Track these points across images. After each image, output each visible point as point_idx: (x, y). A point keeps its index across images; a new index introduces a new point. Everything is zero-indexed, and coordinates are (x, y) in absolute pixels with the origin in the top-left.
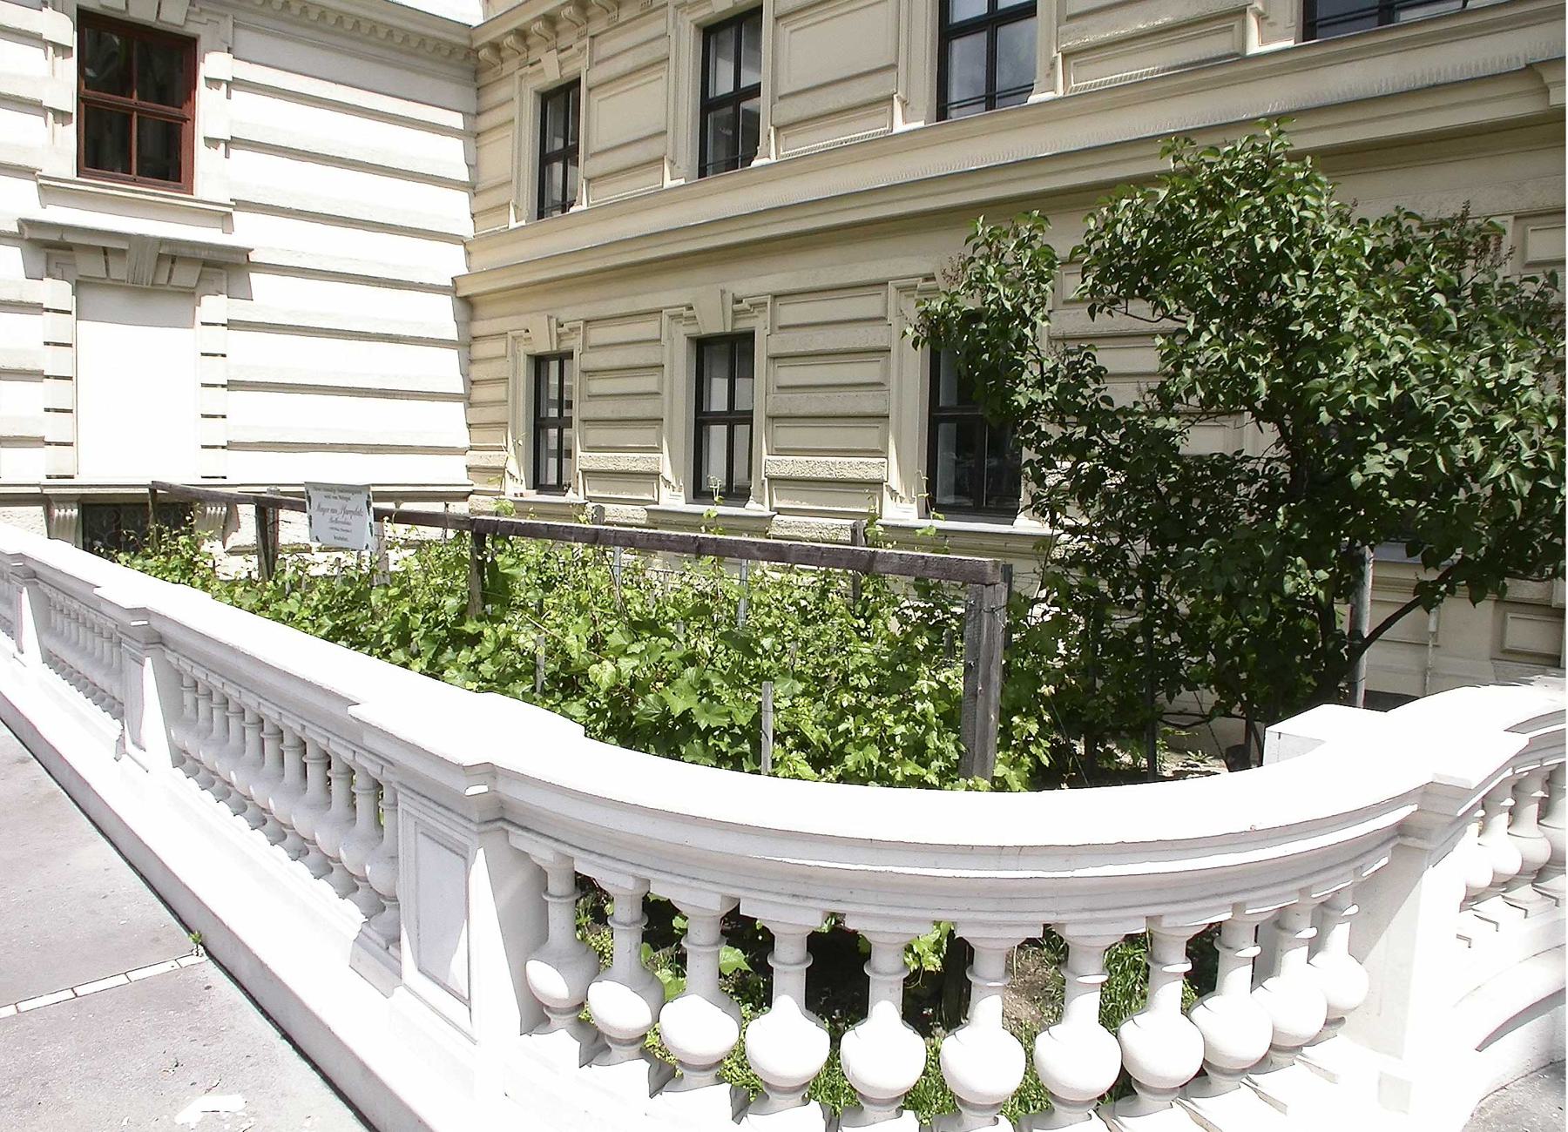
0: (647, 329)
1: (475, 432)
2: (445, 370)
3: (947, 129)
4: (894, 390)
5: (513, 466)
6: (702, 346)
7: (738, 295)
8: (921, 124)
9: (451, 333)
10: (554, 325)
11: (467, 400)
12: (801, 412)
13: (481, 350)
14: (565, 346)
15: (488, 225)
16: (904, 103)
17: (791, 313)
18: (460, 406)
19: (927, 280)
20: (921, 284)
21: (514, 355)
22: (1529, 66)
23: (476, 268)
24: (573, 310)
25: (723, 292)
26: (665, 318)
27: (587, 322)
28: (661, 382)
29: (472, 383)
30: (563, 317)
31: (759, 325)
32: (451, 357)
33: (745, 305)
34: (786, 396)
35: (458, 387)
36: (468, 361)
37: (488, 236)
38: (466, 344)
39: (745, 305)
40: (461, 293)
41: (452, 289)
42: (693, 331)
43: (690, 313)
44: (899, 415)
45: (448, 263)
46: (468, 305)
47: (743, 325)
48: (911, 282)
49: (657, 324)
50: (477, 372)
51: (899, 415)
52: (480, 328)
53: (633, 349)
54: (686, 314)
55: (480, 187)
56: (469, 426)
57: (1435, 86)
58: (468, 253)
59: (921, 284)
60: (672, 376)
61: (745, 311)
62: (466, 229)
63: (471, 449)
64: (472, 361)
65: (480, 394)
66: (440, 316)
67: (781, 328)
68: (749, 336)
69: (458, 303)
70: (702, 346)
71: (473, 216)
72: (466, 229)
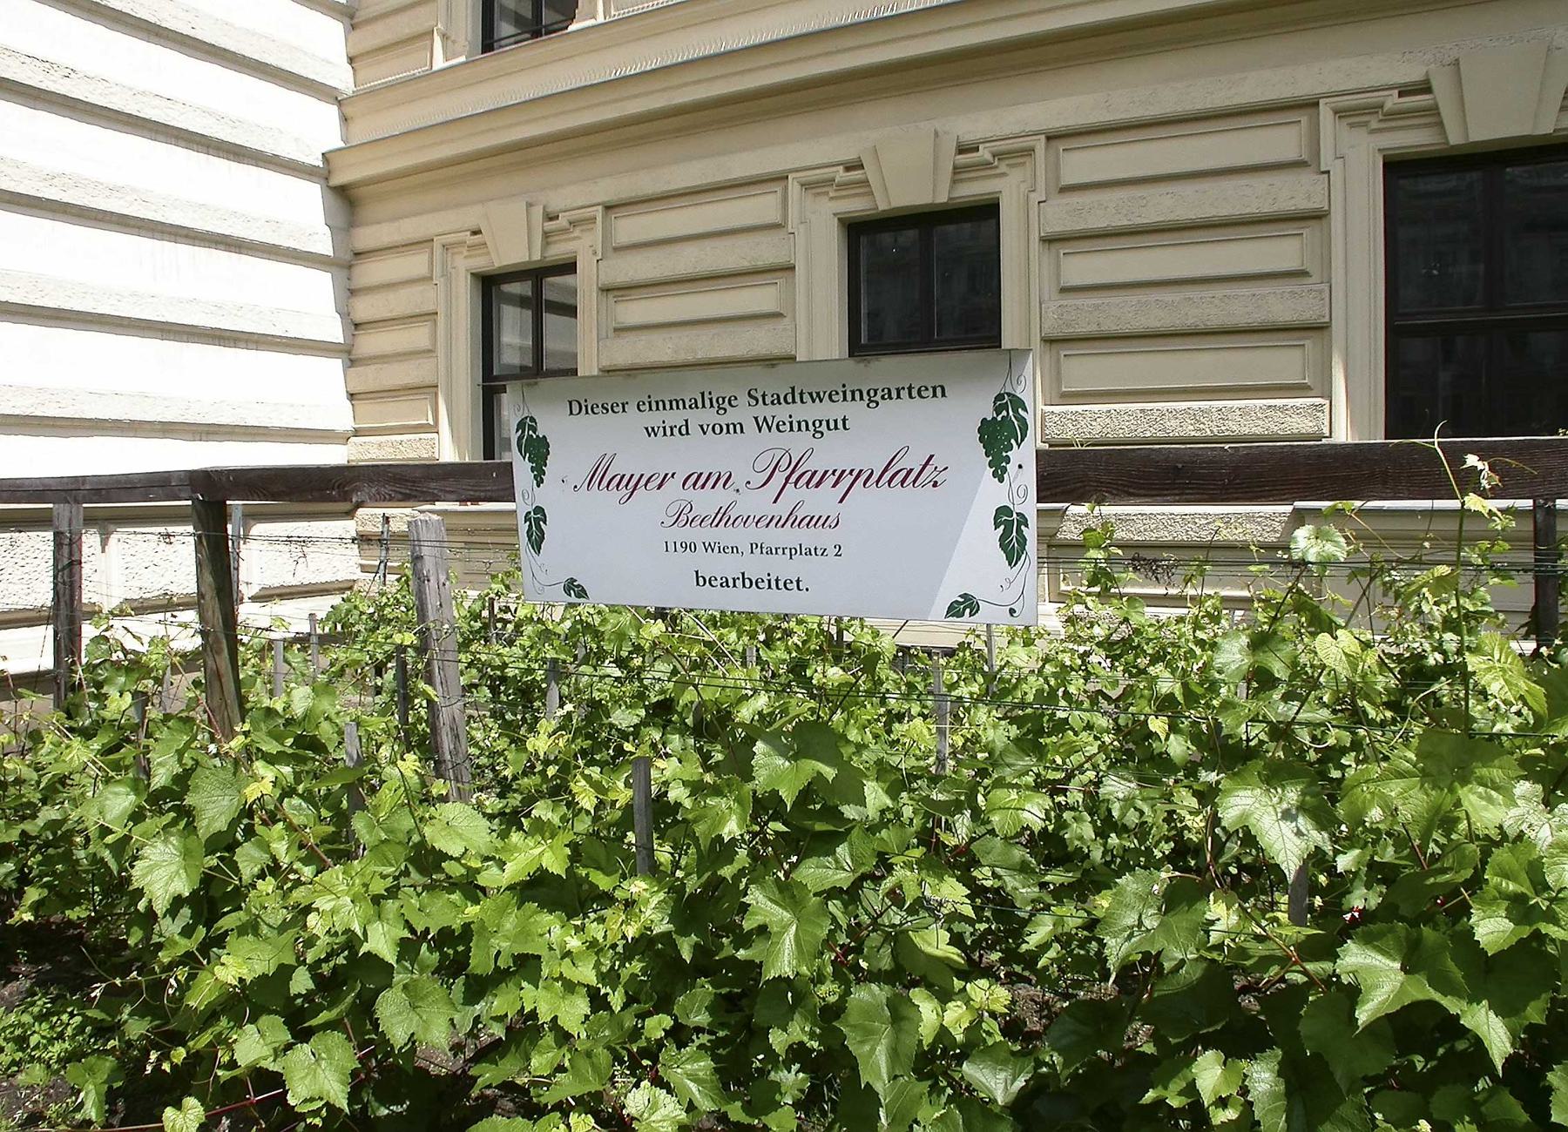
0: (761, 207)
1: (363, 406)
2: (310, 301)
3: (494, 61)
6: (489, 285)
7: (552, 209)
8: (463, 59)
9: (323, 244)
10: (538, 213)
11: (350, 356)
13: (372, 272)
14: (558, 251)
15: (385, 72)
16: (444, 37)
18: (336, 365)
19: (848, 169)
20: (841, 175)
21: (445, 274)
23: (361, 133)
24: (578, 189)
26: (793, 187)
27: (608, 208)
29: (355, 326)
30: (557, 201)
31: (583, 247)
32: (321, 284)
33: (984, 154)
35: (334, 331)
36: (349, 293)
37: (372, 92)
38: (345, 264)
39: (562, 221)
40: (338, 180)
41: (321, 173)
42: (856, 206)
43: (855, 175)
45: (313, 130)
46: (347, 201)
47: (973, 190)
50: (365, 308)
52: (367, 237)
53: (1188, 189)
55: (361, 15)
56: (351, 396)
58: (345, 119)
59: (841, 175)
61: (987, 165)
62: (342, 78)
63: (357, 433)
64: (353, 292)
65: (371, 343)
66: (303, 214)
67: (616, 249)
68: (988, 211)
69: (329, 194)
70: (489, 285)
71: (351, 60)
72: (342, 78)
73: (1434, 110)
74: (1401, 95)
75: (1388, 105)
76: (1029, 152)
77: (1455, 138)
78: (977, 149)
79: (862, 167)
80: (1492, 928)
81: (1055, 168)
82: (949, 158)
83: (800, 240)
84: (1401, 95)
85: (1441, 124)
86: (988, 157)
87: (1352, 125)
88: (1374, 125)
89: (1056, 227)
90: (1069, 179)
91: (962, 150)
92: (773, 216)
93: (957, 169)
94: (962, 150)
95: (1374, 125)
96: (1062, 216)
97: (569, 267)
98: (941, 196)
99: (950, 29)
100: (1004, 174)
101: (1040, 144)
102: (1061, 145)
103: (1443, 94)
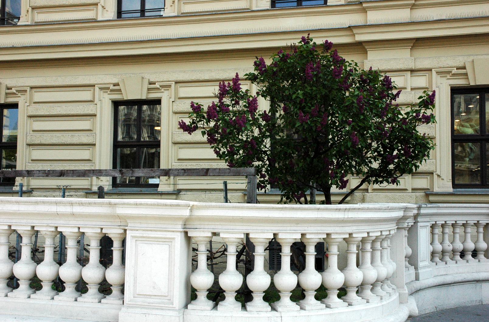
4: (98, 132)
5: (427, 168)
12: (47, 142)
17: (39, 96)
19: (114, 85)
20: (112, 87)
22: (349, 27)
25: (143, 78)
28: (94, 124)
31: (21, 100)
33: (157, 85)
34: (38, 134)
44: (100, 143)
48: (449, 69)
49: (92, 92)
51: (100, 143)
54: (116, 88)
57: (162, 39)
59: (112, 87)
60: (101, 121)
61: (14, 94)
73: (466, 74)
74: (457, 69)
75: (453, 72)
76: (26, 91)
77: (472, 83)
78: (155, 84)
79: (119, 85)
80: (410, 212)
81: (31, 97)
82: (146, 86)
83: (99, 106)
84: (457, 69)
85: (468, 78)
86: (15, 91)
87: (441, 77)
88: (109, 93)
89: (31, 113)
90: (182, 95)
91: (150, 83)
92: (89, 98)
93: (149, 89)
94: (150, 83)
95: (448, 77)
96: (33, 110)
97: (158, 102)
98: (144, 96)
99: (469, 26)
100: (163, 92)
101: (28, 89)
102: (34, 90)
103: (469, 70)
